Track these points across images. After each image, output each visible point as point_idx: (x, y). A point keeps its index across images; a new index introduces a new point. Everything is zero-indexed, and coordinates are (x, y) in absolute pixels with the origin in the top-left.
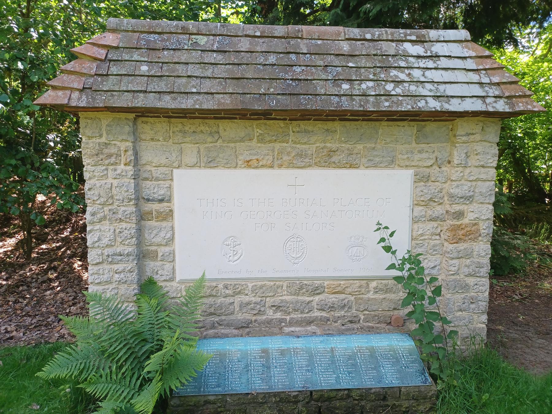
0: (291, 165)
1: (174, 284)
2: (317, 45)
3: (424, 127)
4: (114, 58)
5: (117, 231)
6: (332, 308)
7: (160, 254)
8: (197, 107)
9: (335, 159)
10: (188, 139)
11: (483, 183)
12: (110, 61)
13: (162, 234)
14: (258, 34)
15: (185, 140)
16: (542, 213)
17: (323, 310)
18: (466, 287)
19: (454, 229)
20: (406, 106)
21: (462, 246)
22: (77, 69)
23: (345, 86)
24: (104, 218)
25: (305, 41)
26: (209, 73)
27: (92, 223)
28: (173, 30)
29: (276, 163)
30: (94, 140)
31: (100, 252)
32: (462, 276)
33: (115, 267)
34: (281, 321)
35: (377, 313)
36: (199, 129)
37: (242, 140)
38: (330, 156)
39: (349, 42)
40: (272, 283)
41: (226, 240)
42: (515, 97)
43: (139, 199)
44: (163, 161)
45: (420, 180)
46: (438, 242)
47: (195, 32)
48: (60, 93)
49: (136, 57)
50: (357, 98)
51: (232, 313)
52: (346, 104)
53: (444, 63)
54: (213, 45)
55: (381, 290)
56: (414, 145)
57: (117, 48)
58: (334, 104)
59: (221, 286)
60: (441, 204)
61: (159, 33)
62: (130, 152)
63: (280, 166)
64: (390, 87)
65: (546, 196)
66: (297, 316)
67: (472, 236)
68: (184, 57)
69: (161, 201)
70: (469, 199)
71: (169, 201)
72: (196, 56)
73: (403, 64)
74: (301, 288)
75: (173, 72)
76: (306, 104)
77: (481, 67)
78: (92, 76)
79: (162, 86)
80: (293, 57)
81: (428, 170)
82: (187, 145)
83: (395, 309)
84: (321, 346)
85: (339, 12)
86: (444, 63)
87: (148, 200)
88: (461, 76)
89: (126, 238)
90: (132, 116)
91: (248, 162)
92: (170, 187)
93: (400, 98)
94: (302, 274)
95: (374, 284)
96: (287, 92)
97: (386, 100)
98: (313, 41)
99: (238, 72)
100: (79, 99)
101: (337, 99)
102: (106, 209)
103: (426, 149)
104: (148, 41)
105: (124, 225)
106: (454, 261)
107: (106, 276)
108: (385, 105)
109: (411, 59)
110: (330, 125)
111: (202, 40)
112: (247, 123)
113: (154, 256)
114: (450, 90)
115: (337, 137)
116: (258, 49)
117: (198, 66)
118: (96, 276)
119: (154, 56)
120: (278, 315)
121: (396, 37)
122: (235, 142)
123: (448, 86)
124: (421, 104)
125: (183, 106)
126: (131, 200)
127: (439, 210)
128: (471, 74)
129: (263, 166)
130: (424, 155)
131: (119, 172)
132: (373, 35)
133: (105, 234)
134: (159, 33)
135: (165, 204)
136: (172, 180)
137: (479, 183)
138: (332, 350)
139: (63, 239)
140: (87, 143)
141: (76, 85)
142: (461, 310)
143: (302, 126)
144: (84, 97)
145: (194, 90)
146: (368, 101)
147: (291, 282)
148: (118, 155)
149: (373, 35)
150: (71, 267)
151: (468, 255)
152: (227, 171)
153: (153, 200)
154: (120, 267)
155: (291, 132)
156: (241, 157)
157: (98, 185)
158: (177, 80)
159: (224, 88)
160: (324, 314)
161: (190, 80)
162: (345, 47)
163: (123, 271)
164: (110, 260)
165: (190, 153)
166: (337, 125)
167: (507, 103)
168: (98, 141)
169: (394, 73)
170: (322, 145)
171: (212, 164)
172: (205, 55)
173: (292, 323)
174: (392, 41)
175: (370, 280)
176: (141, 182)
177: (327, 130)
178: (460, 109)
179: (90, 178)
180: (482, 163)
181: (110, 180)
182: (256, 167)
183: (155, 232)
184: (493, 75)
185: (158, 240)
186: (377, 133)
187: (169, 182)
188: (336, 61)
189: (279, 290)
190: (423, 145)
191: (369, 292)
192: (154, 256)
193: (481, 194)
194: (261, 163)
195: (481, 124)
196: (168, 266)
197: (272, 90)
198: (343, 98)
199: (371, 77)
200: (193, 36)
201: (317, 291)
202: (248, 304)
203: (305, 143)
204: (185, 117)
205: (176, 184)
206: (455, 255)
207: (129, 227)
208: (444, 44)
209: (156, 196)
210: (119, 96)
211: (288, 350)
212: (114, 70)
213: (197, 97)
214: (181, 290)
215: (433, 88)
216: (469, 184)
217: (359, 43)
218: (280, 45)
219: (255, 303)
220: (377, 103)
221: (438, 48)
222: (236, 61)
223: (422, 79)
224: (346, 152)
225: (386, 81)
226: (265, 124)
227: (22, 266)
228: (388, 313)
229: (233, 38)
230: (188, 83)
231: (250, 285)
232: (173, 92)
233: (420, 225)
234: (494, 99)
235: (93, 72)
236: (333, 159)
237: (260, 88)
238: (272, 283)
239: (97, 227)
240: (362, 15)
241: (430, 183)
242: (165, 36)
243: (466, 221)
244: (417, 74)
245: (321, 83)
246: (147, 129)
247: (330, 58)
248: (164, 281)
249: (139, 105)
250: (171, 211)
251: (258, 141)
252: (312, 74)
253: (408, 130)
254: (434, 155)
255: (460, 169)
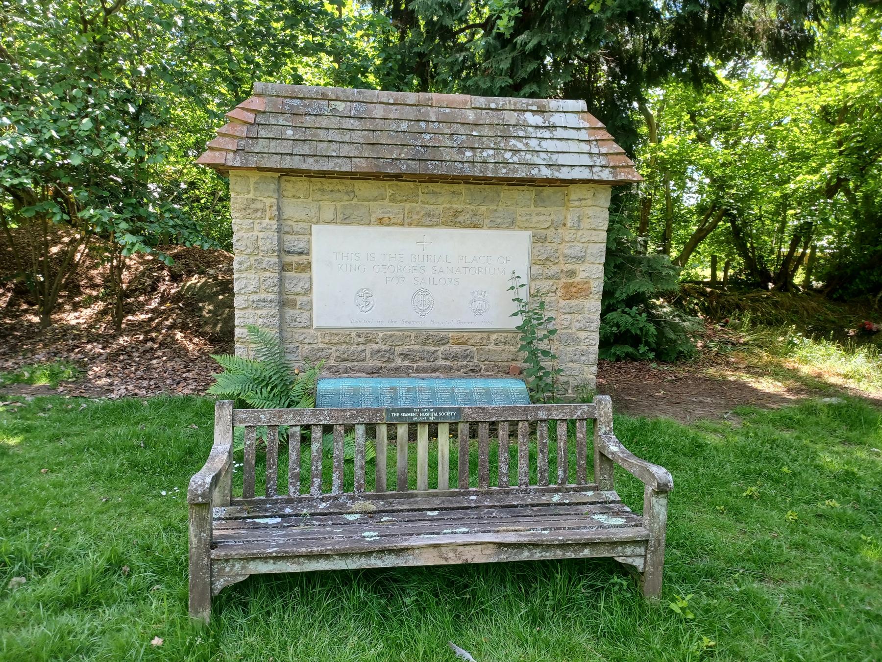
0: (420, 224)
1: (311, 331)
2: (445, 113)
3: (541, 192)
4: (263, 122)
5: (262, 279)
6: (455, 357)
7: (299, 303)
8: (337, 169)
9: (461, 219)
10: (325, 197)
11: (595, 245)
12: (259, 124)
13: (301, 284)
14: (392, 101)
15: (324, 198)
16: (758, 300)
17: (447, 359)
18: (577, 341)
19: (567, 286)
20: (521, 174)
21: (574, 302)
22: (231, 132)
23: (469, 154)
24: (250, 267)
25: (435, 109)
26: (347, 138)
27: (239, 271)
28: (314, 96)
29: (406, 221)
30: (242, 196)
31: (246, 298)
32: (574, 330)
33: (260, 312)
34: (408, 368)
35: (496, 363)
36: (336, 188)
37: (375, 199)
38: (456, 217)
39: (475, 111)
40: (401, 333)
41: (358, 292)
42: (619, 167)
43: (283, 251)
44: (304, 217)
45: (538, 241)
46: (553, 299)
47: (334, 98)
48: (217, 154)
49: (282, 122)
50: (478, 165)
51: (364, 360)
52: (468, 170)
53: (559, 133)
54: (350, 111)
55: (501, 342)
56: (532, 207)
57: (264, 112)
58: (458, 169)
59: (354, 334)
60: (556, 263)
61: (300, 98)
62: (275, 208)
63: (410, 225)
64: (508, 155)
65: (770, 279)
66: (423, 364)
67: (583, 293)
68: (324, 123)
69: (301, 253)
70: (581, 259)
71: (308, 254)
72: (334, 122)
73: (521, 134)
74: (427, 338)
75: (316, 136)
76: (433, 170)
77: (592, 138)
78: (244, 139)
79: (306, 149)
80: (423, 124)
81: (545, 232)
82: (326, 203)
83: (513, 360)
84: (443, 386)
85: (491, 41)
86: (559, 133)
87: (289, 252)
88: (573, 146)
89: (270, 287)
90: (277, 175)
91: (381, 219)
92: (309, 241)
93: (517, 166)
94: (428, 325)
95: (494, 337)
96: (417, 158)
97: (504, 168)
98: (442, 110)
99: (373, 137)
100: (234, 159)
101: (460, 165)
102: (252, 259)
103: (543, 212)
104: (292, 106)
105: (268, 274)
106: (566, 316)
107: (251, 320)
108: (503, 172)
109: (530, 129)
110: (456, 186)
111: (341, 106)
112: (380, 183)
113: (293, 304)
114: (562, 159)
115: (462, 200)
116: (391, 116)
117: (337, 131)
118: (242, 320)
119: (298, 121)
120: (406, 363)
121: (519, 107)
122: (369, 201)
123: (560, 155)
124: (535, 172)
125: (325, 169)
126: (274, 251)
127: (554, 269)
128: (583, 144)
129: (394, 224)
130: (542, 218)
131: (264, 225)
132: (497, 104)
133: (250, 284)
134: (300, 98)
135: (304, 257)
136: (310, 234)
137: (591, 245)
138: (452, 389)
139: (152, 311)
140: (236, 199)
141: (230, 147)
142: (572, 361)
143: (431, 188)
144: (238, 158)
145: (334, 154)
146: (487, 168)
147: (419, 331)
148: (264, 210)
149: (497, 104)
150: (173, 338)
151: (580, 311)
152: (362, 228)
153: (293, 253)
154: (264, 312)
155: (420, 193)
156: (374, 215)
157: (245, 237)
158: (319, 144)
159: (361, 153)
160: (448, 363)
161: (331, 144)
162: (471, 116)
163: (267, 316)
164: (255, 305)
165: (328, 212)
166: (462, 188)
167: (611, 173)
168: (246, 196)
169: (513, 142)
170: (449, 206)
171: (347, 221)
172: (343, 121)
173: (418, 370)
174: (514, 110)
175: (490, 332)
176: (282, 235)
177: (453, 192)
178: (569, 177)
179: (238, 231)
180: (593, 226)
181: (256, 233)
182: (388, 225)
183: (295, 282)
184: (603, 146)
185: (297, 289)
186: (499, 196)
187: (308, 236)
188: (462, 130)
189: (407, 340)
190: (541, 209)
191: (489, 343)
192: (293, 304)
193: (592, 254)
194: (392, 221)
195: (593, 190)
196: (306, 314)
197: (403, 155)
198: (466, 164)
199: (492, 145)
200: (332, 102)
201: (441, 342)
202: (379, 351)
203: (433, 204)
204: (325, 177)
205: (314, 238)
206: (568, 310)
207: (273, 276)
208: (563, 114)
209: (296, 249)
210: (269, 158)
211: (414, 388)
212: (263, 133)
213: (337, 160)
214: (317, 337)
215: (546, 157)
216: (581, 245)
217: (484, 112)
218: (411, 113)
219: (385, 351)
220: (496, 170)
221: (557, 119)
222: (371, 128)
223: (538, 149)
224: (471, 213)
225: (506, 150)
226: (397, 185)
227: (114, 337)
228: (507, 364)
229: (369, 105)
230: (329, 147)
231: (381, 335)
232: (316, 156)
233: (538, 283)
234: (600, 168)
235: (244, 135)
236: (459, 219)
237: (392, 152)
238: (401, 333)
239: (244, 275)
240: (518, 46)
241: (547, 244)
242: (307, 102)
243: (577, 279)
244: (533, 143)
245: (447, 150)
246: (290, 186)
247: (456, 127)
248: (302, 327)
249: (286, 166)
250: (309, 263)
251: (390, 201)
252: (439, 141)
253: (526, 194)
254: (551, 218)
255: (573, 231)
